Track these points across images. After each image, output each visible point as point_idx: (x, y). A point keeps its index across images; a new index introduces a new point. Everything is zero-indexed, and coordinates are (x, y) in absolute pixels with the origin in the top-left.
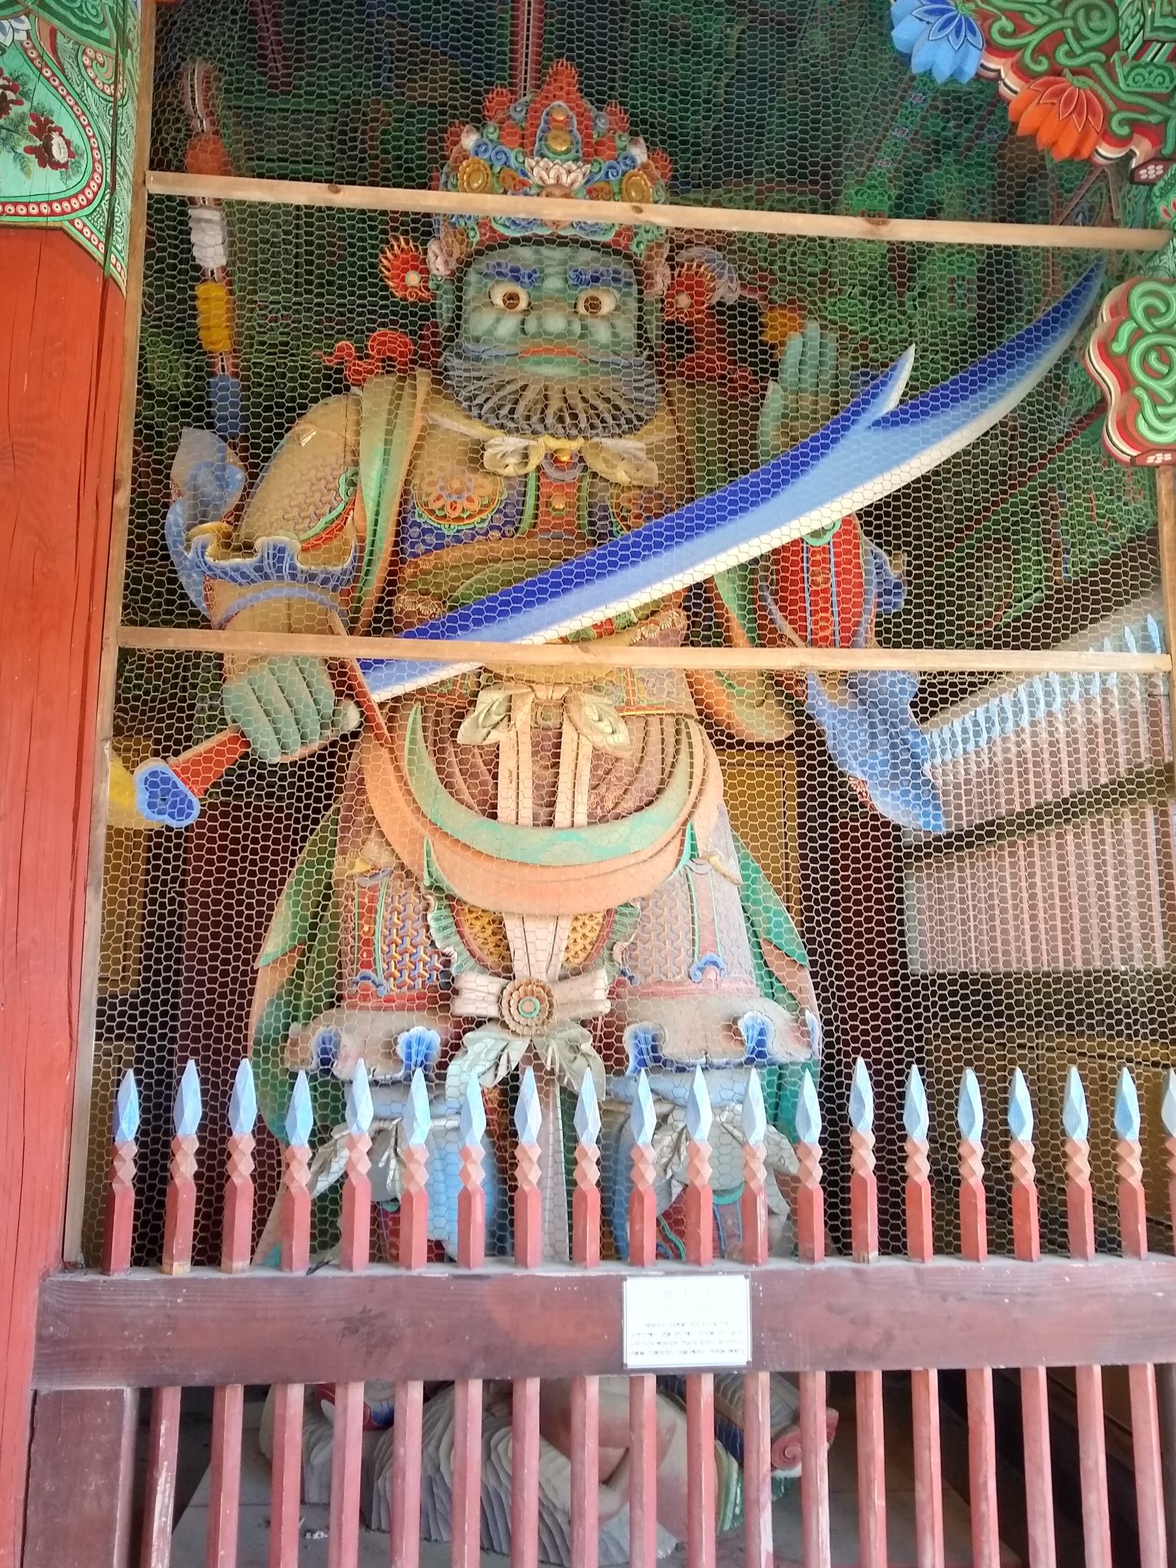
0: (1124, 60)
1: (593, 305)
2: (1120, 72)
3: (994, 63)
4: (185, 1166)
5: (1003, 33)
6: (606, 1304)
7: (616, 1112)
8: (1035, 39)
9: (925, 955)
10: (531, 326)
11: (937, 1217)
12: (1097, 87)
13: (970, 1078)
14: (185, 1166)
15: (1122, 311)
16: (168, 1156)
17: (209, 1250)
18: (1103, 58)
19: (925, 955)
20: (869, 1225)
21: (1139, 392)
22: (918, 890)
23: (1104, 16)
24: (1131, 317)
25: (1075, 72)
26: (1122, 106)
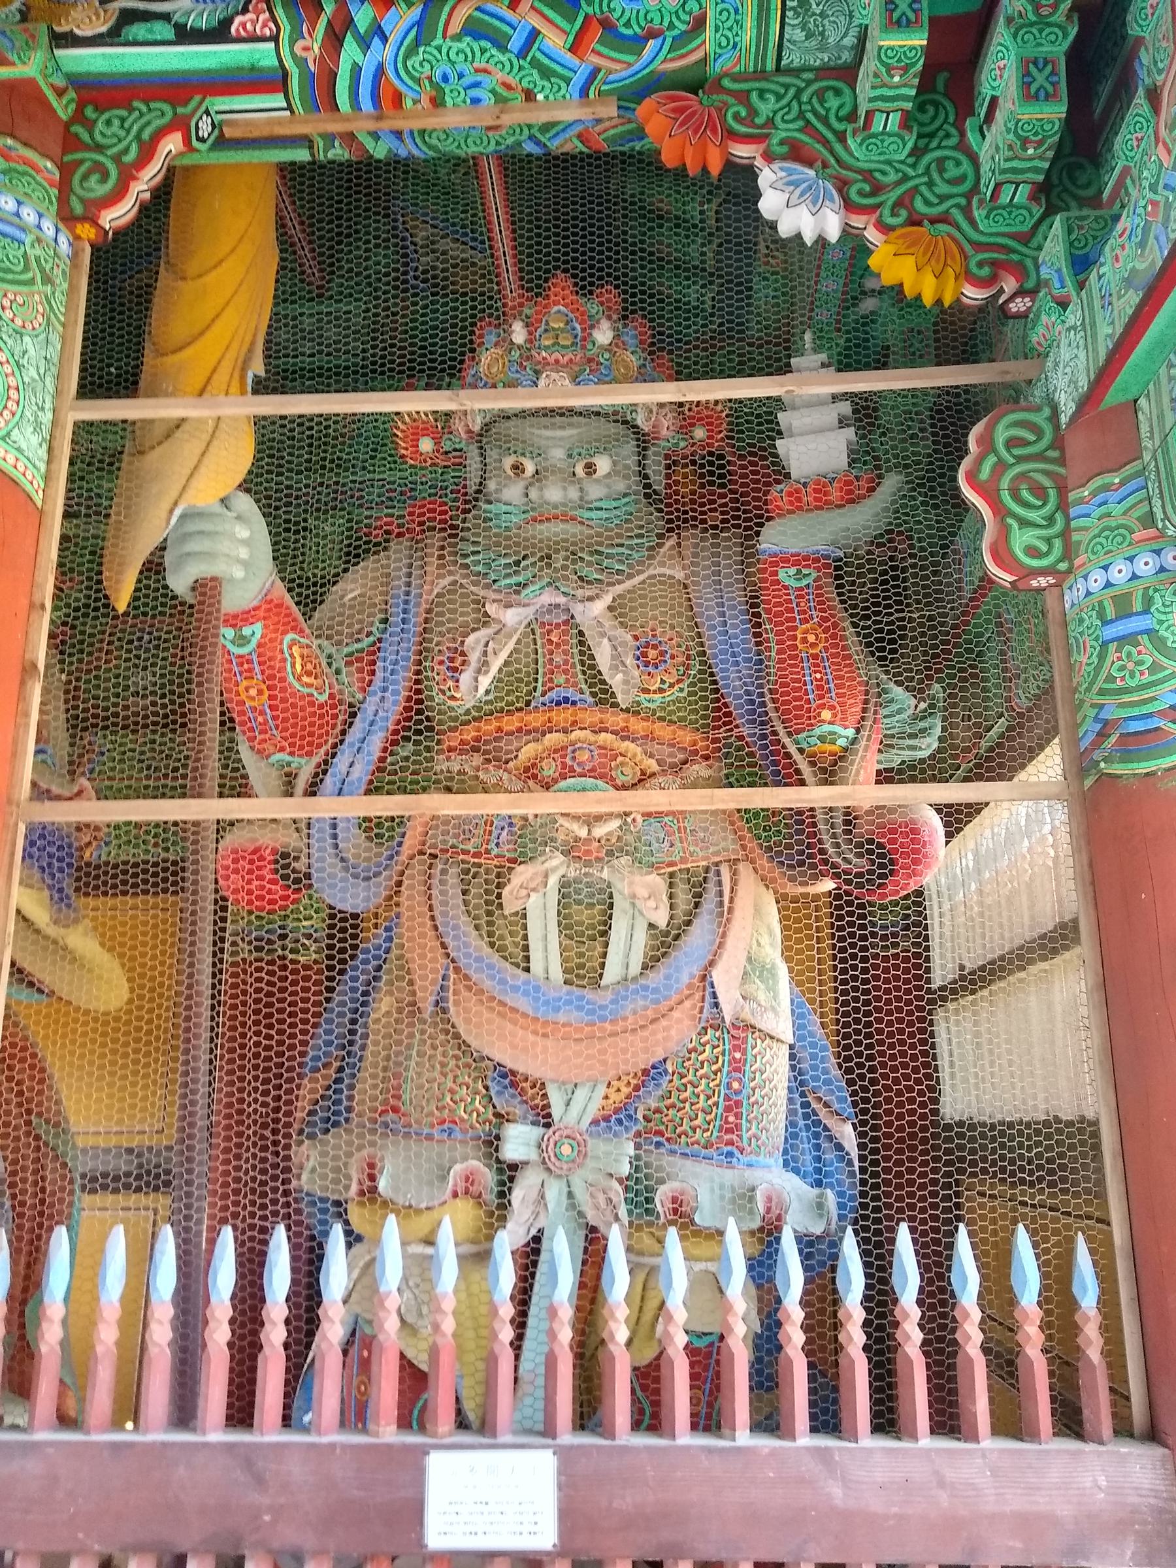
0: (981, 202)
1: (590, 468)
2: (977, 214)
3: (858, 221)
4: (855, 1336)
5: (860, 193)
6: (412, 1466)
7: (647, 1276)
8: (893, 196)
9: (958, 1101)
10: (534, 494)
11: (874, 1390)
12: (957, 235)
13: (1023, 1240)
14: (855, 1336)
15: (987, 442)
16: (837, 1326)
17: (241, 1412)
18: (963, 201)
19: (958, 1101)
20: (980, 1406)
21: (1010, 521)
22: (953, 1031)
23: (958, 164)
24: (994, 451)
25: (933, 221)
26: (979, 247)
